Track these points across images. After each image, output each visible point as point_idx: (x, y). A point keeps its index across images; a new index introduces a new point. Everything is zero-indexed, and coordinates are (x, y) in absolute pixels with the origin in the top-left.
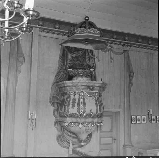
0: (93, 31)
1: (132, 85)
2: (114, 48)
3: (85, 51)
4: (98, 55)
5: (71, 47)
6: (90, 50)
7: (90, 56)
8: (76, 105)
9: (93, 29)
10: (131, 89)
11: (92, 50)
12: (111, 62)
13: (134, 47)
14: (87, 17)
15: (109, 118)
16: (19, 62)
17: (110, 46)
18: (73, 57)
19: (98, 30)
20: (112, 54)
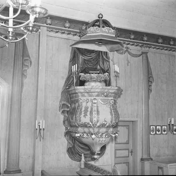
0: (108, 30)
1: (151, 91)
2: (130, 50)
3: (99, 53)
6: (104, 52)
7: (104, 58)
8: (88, 113)
11: (106, 52)
20: (129, 56)
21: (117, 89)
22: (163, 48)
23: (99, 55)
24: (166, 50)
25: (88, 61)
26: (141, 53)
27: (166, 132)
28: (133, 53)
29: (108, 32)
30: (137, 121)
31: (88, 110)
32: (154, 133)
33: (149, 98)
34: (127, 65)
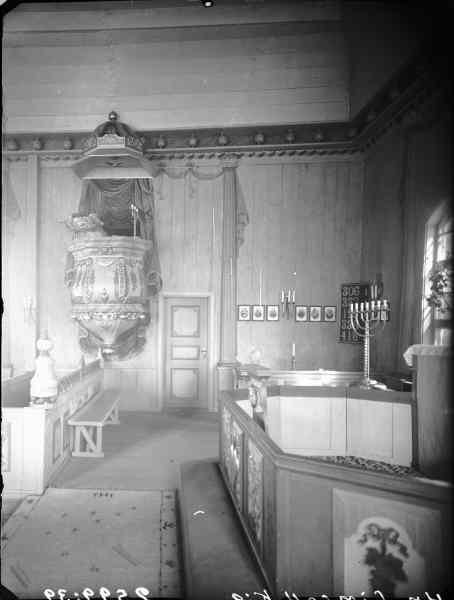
1: (243, 241)
5: (103, 180)
14: (113, 113)
15: (192, 310)
18: (107, 198)
23: (133, 188)
24: (301, 154)
25: (115, 199)
27: (255, 312)
31: (429, 308)
32: (248, 318)
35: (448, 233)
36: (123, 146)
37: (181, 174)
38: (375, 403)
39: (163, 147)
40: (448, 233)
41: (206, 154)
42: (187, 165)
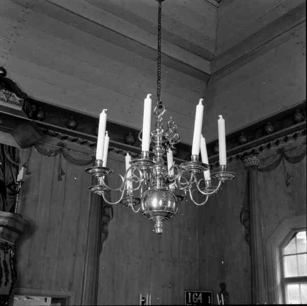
0: (6, 96)
1: (107, 234)
2: (69, 149)
4: (29, 160)
6: (9, 147)
7: (7, 160)
9: (7, 92)
10: (104, 245)
11: (14, 148)
12: (60, 179)
13: (118, 152)
16: (10, 295)
17: (60, 143)
19: (18, 96)
20: (64, 161)
21: (11, 218)
22: (137, 154)
26: (91, 159)
28: (75, 158)
29: (6, 100)
30: (69, 297)
33: (99, 249)
34: (57, 179)
35: (300, 285)
36: (20, 109)
37: (51, 152)
38: (194, 139)
39: (41, 120)
40: (300, 285)
41: (80, 139)
42: (59, 144)
